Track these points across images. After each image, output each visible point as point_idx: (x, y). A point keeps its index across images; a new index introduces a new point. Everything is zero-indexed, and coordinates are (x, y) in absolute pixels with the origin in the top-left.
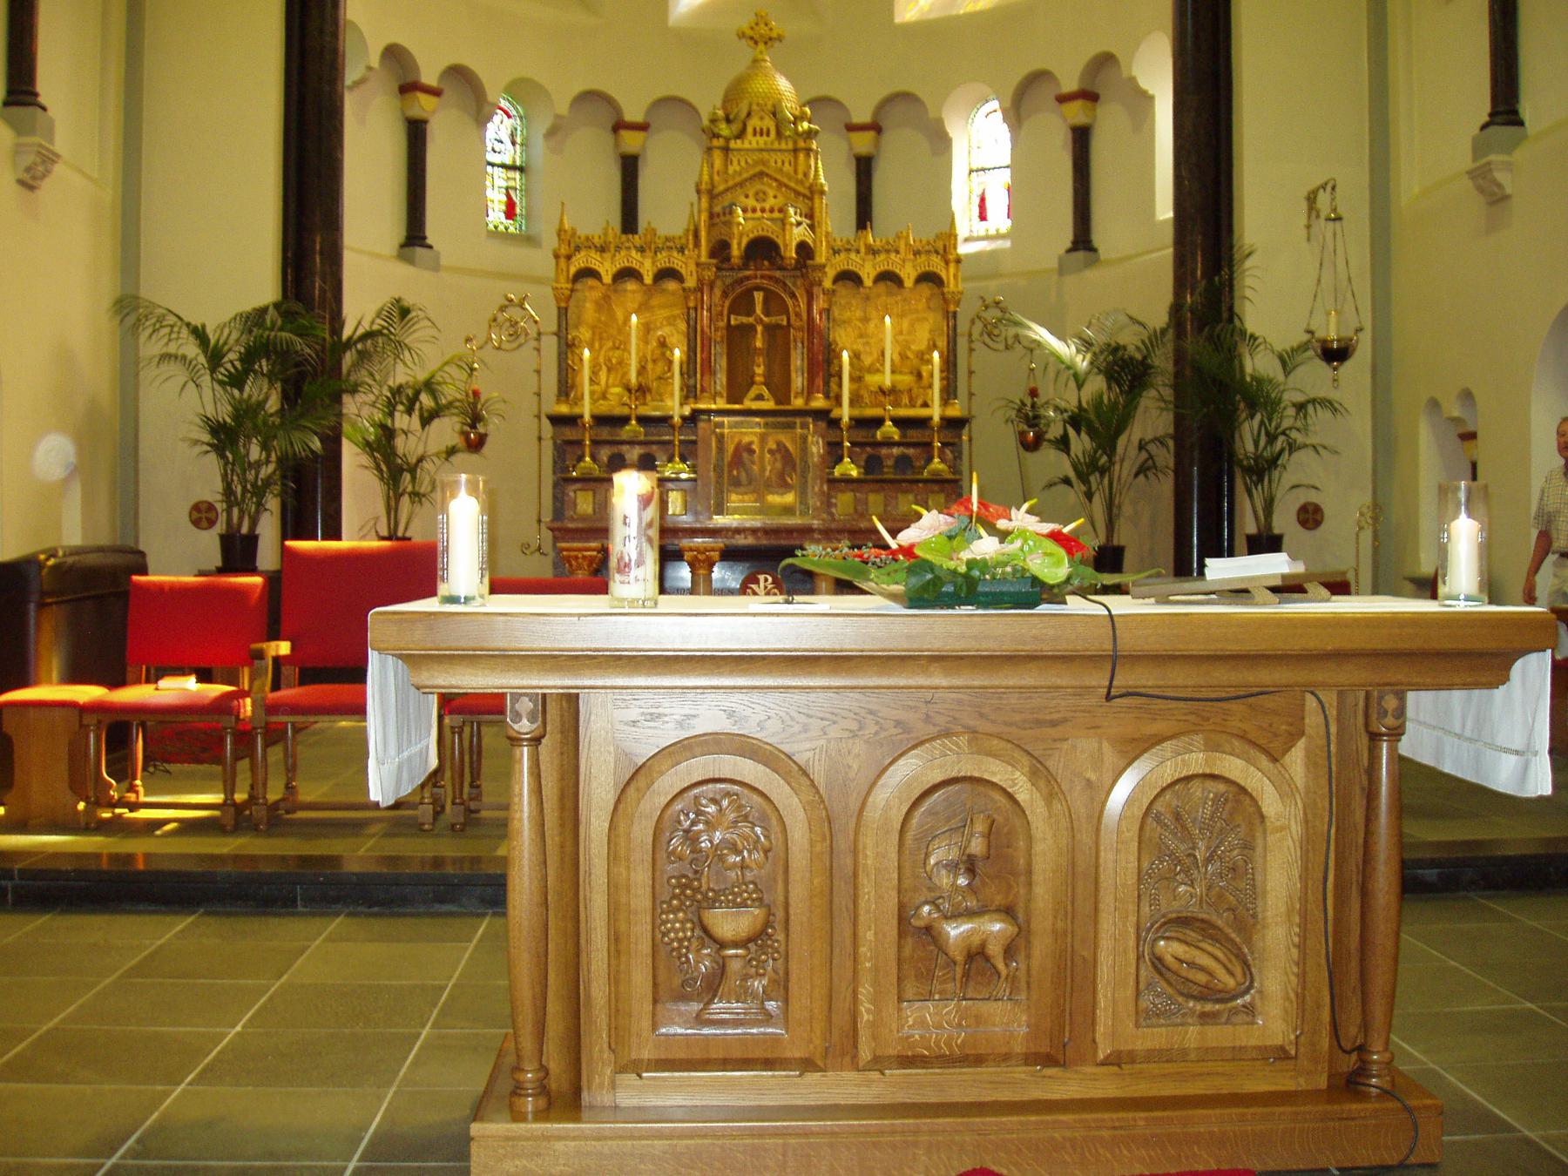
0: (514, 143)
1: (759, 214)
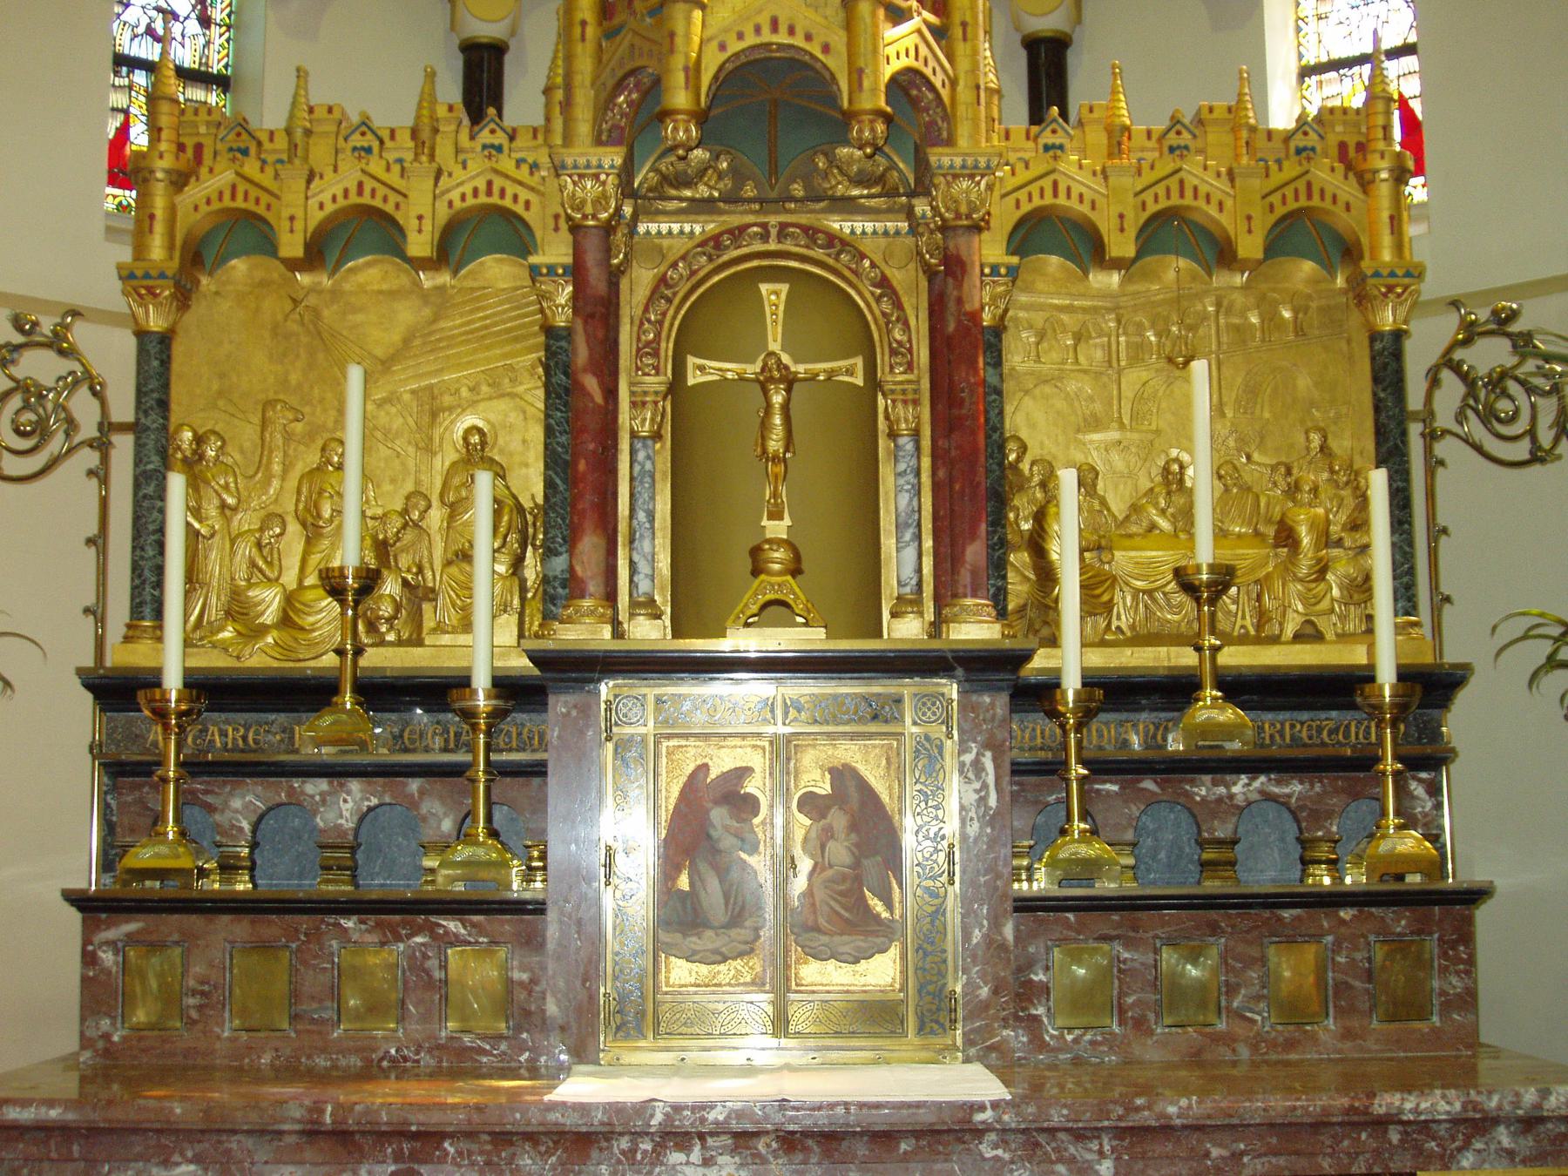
0: (205, 21)
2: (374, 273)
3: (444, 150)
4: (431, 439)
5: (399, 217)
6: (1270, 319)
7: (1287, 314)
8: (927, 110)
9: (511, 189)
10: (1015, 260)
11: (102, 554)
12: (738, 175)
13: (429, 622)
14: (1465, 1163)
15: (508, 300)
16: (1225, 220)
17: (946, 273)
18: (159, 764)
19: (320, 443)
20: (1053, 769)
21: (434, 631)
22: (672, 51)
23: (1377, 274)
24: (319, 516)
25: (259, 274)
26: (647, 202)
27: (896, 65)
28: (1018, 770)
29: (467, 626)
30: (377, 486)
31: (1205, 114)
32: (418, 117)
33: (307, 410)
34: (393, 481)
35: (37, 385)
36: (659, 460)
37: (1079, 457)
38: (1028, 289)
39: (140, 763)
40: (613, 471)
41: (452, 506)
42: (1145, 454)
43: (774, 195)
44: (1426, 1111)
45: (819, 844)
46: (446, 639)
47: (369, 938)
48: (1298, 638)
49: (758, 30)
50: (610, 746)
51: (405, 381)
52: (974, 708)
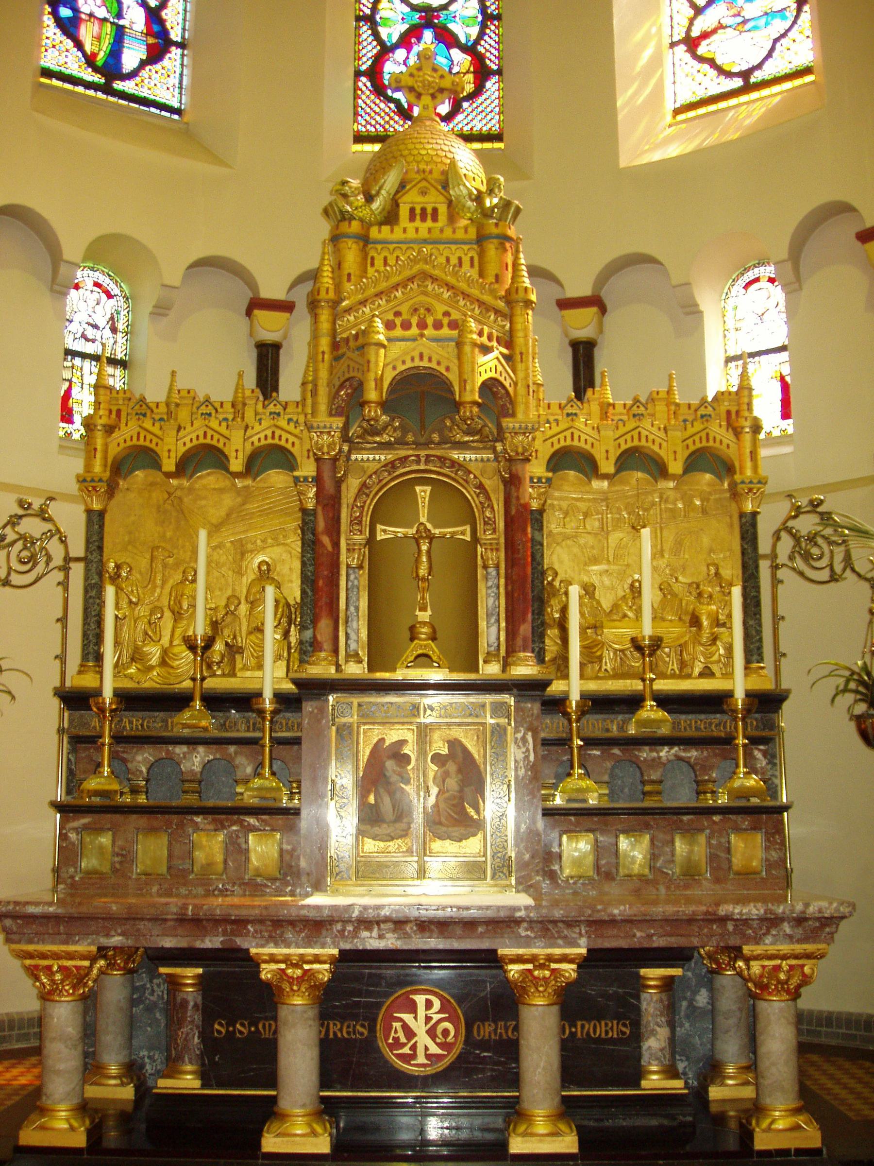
0: (114, 330)
1: (414, 331)
2: (211, 478)
3: (249, 413)
4: (241, 567)
5: (226, 450)
6: (689, 504)
7: (698, 503)
8: (501, 398)
9: (285, 436)
10: (550, 475)
11: (65, 627)
12: (404, 429)
13: (239, 665)
14: (767, 941)
15: (282, 494)
16: (662, 453)
17: (512, 482)
18: (100, 737)
19: (182, 569)
20: (564, 742)
21: (242, 669)
22: (368, 370)
23: (743, 482)
24: (181, 608)
25: (151, 479)
26: (354, 447)
27: (485, 377)
28: (546, 743)
29: (260, 667)
30: (212, 592)
31: (655, 395)
32: (235, 397)
33: (175, 551)
34: (221, 589)
35: (31, 537)
36: (362, 579)
37: (586, 579)
38: (558, 489)
39: (88, 737)
40: (338, 586)
41: (252, 603)
42: (623, 574)
43: (422, 440)
44: (746, 914)
45: (441, 780)
46: (248, 674)
47: (208, 827)
48: (701, 675)
49: (413, 359)
50: (334, 728)
51: (228, 537)
52: (522, 710)
